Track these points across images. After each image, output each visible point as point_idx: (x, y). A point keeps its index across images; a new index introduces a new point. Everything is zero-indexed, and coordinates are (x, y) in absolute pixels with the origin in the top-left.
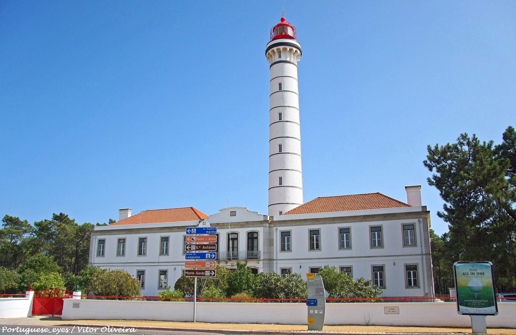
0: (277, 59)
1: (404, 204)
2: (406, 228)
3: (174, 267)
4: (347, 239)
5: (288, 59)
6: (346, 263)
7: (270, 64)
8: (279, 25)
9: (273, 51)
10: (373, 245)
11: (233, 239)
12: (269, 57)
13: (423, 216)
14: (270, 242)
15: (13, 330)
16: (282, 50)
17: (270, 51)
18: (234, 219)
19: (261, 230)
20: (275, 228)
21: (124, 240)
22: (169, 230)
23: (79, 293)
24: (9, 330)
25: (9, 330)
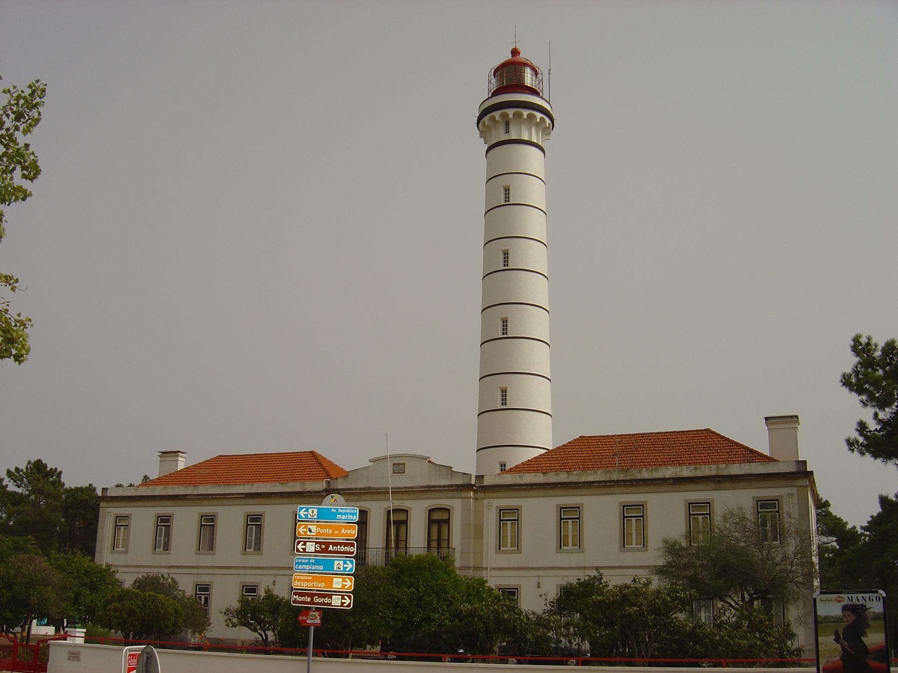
1: (761, 455)
3: (272, 579)
5: (526, 138)
7: (486, 147)
9: (493, 118)
11: (398, 523)
13: (800, 482)
16: (511, 116)
17: (486, 119)
18: (402, 482)
20: (486, 501)
21: (516, 510)
22: (713, 486)
23: (80, 632)
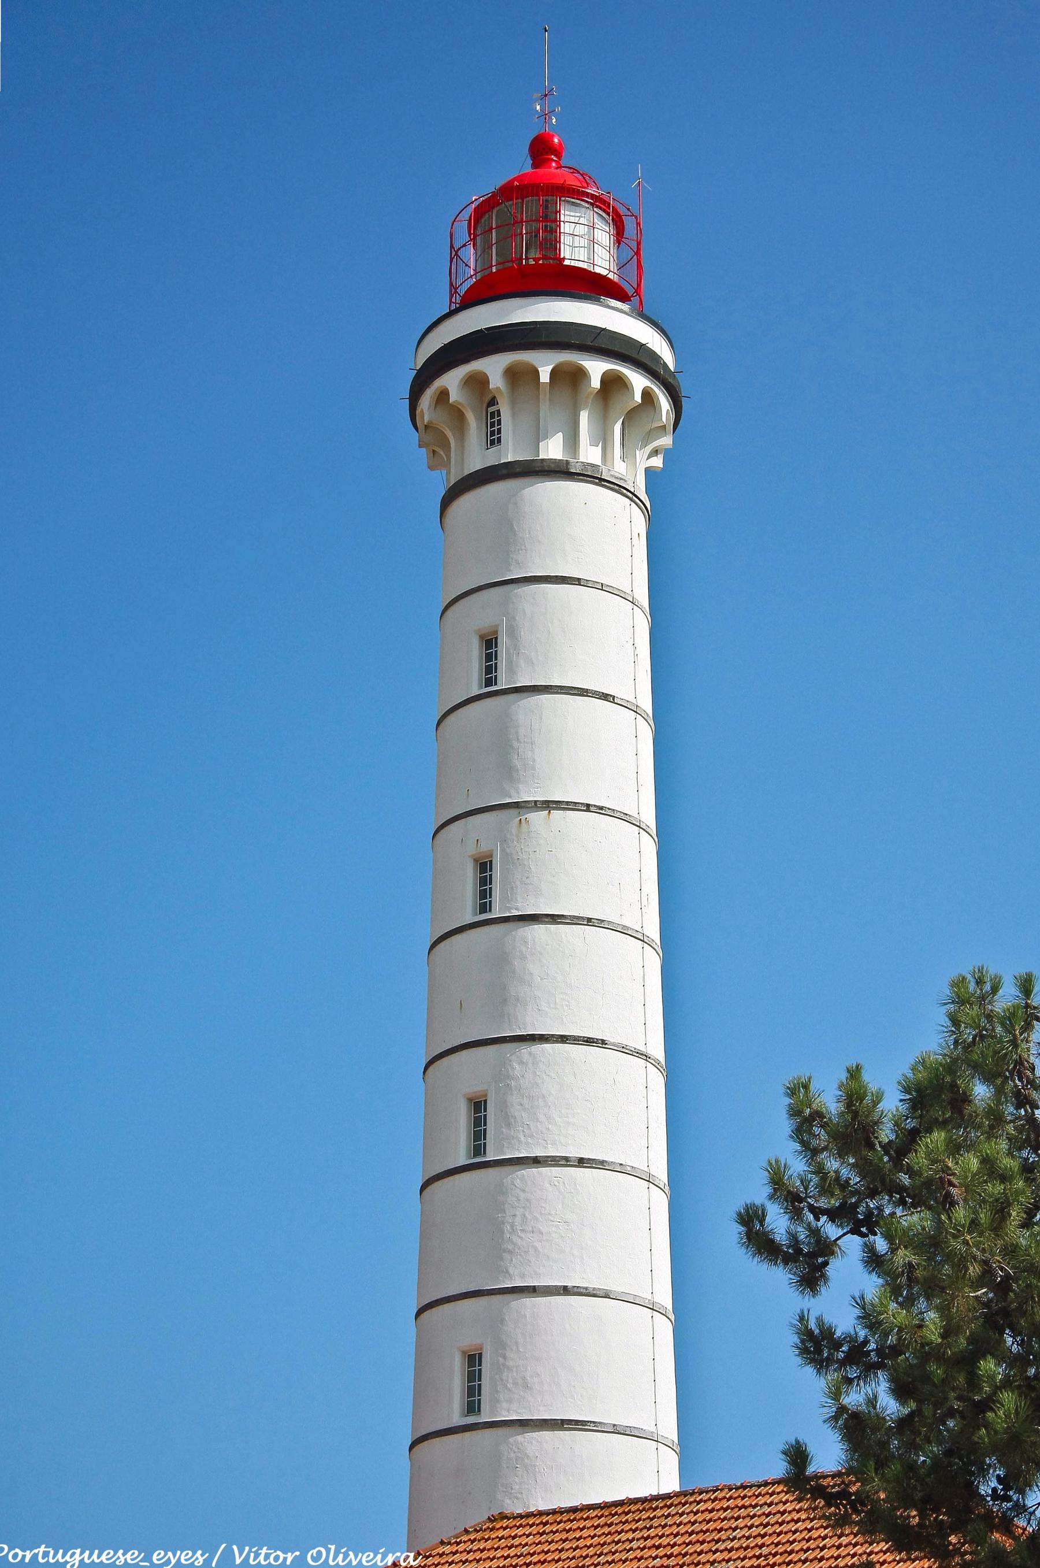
0: (477, 457)
5: (553, 449)
8: (509, 192)
12: (436, 444)
15: (28, 1555)
16: (545, 377)
24: (15, 1556)
25: (15, 1556)
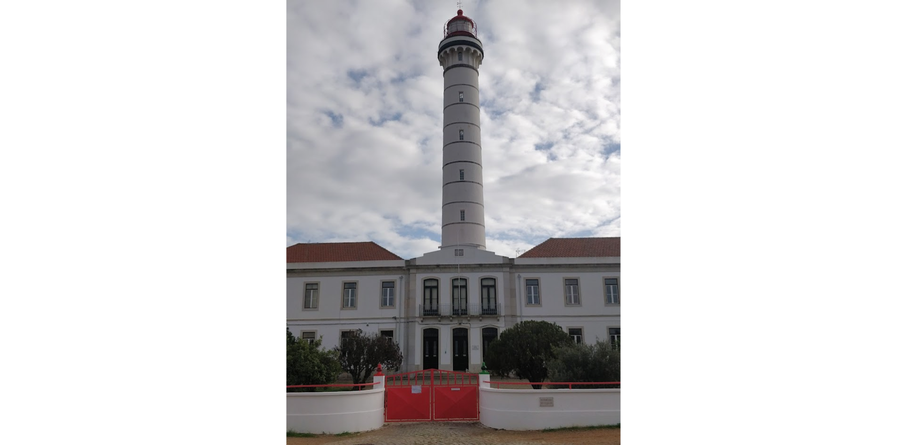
0: (457, 62)
2: (309, 287)
4: (352, 296)
5: (471, 64)
6: (575, 324)
10: (568, 302)
14: (511, 293)
19: (500, 277)
20: (516, 275)
